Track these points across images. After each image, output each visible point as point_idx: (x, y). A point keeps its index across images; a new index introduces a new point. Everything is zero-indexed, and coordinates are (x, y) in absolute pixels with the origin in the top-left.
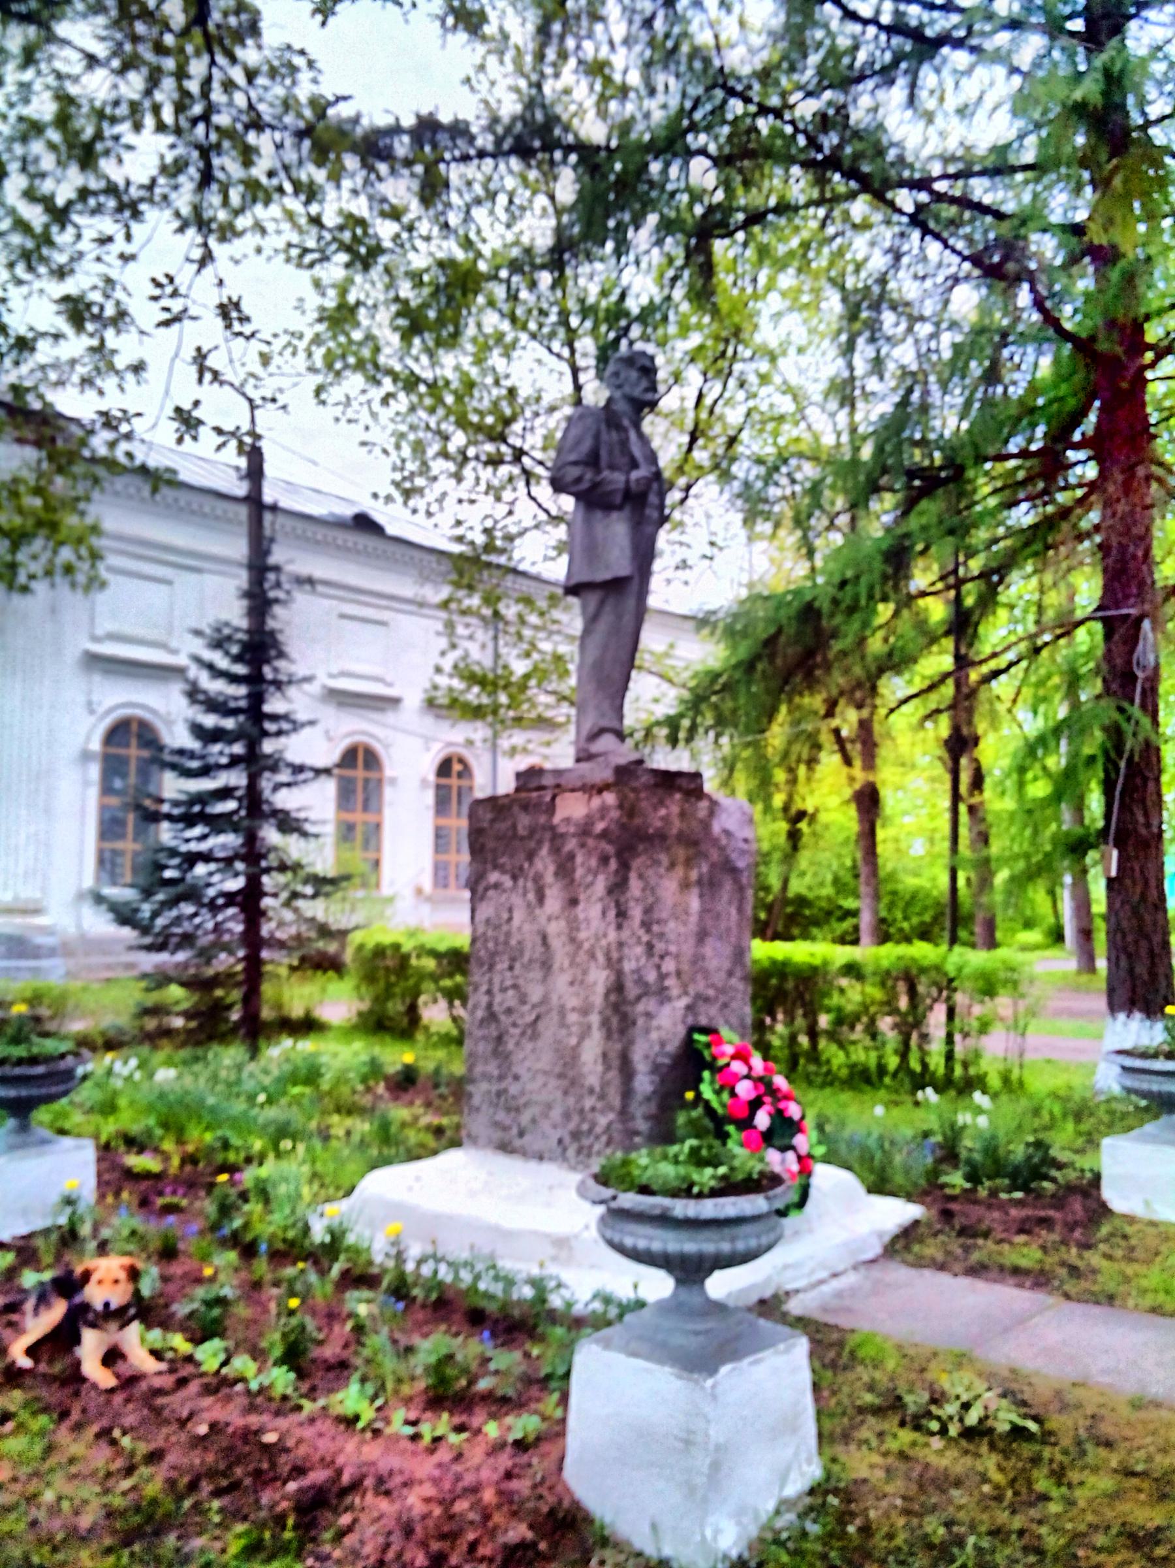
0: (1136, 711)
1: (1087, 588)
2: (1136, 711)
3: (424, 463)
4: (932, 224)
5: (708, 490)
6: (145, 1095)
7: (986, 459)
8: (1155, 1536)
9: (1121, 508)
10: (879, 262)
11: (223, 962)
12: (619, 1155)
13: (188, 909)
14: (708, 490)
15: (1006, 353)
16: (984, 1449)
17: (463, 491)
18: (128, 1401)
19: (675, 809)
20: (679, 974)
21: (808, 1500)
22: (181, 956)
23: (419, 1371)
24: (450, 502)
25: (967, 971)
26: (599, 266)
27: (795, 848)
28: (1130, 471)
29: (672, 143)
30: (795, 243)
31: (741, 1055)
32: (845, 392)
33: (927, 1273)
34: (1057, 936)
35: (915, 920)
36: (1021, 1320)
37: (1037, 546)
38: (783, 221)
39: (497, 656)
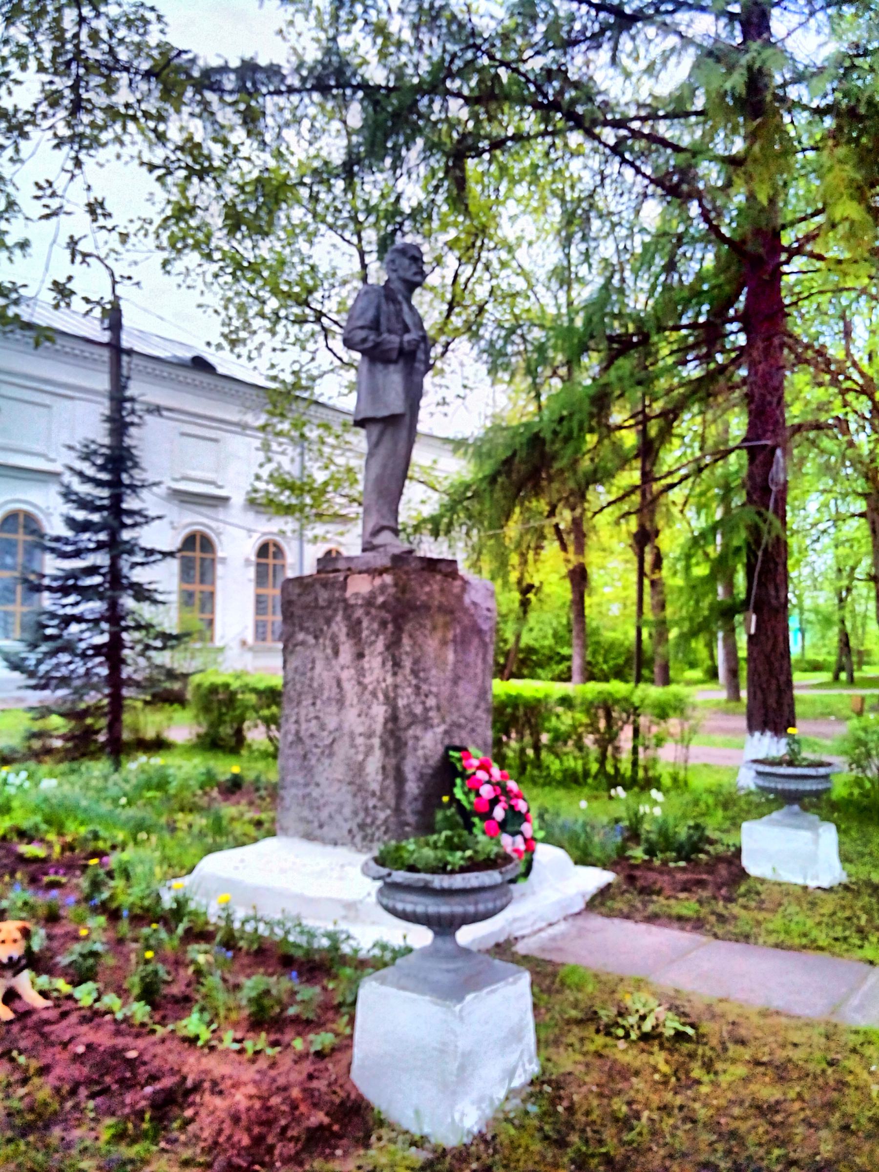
0: (770, 515)
1: (738, 424)
2: (770, 515)
3: (246, 321)
4: (627, 156)
5: (462, 346)
6: (33, 799)
7: (665, 329)
8: (775, 1107)
9: (761, 367)
10: (588, 181)
11: (92, 698)
12: (393, 843)
13: (64, 658)
14: (462, 346)
15: (680, 251)
16: (656, 1049)
17: (277, 342)
18: (23, 1029)
19: (436, 587)
20: (438, 708)
21: (530, 1089)
22: (62, 692)
23: (244, 1002)
24: (266, 350)
25: (647, 702)
26: (379, 176)
27: (525, 612)
28: (769, 339)
29: (435, 86)
30: (527, 162)
31: (484, 766)
32: (564, 277)
33: (617, 921)
34: (713, 674)
35: (611, 663)
36: (683, 954)
37: (701, 394)
38: (518, 147)
39: (303, 468)
